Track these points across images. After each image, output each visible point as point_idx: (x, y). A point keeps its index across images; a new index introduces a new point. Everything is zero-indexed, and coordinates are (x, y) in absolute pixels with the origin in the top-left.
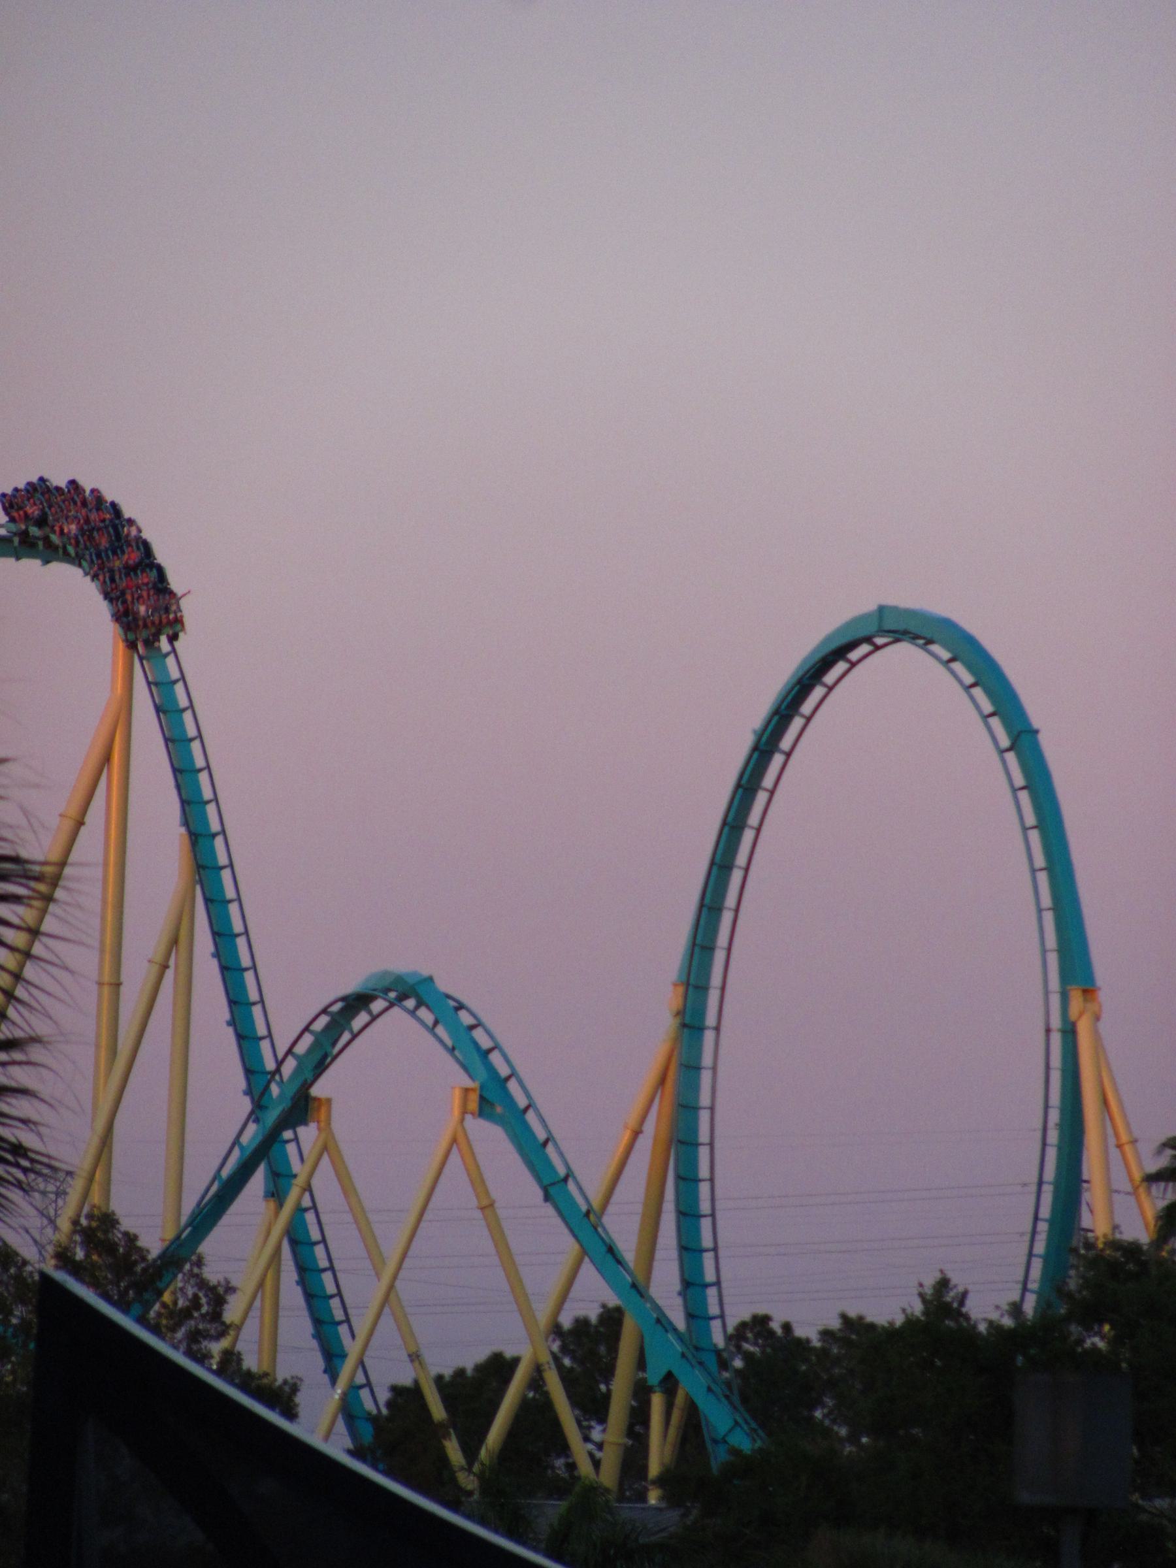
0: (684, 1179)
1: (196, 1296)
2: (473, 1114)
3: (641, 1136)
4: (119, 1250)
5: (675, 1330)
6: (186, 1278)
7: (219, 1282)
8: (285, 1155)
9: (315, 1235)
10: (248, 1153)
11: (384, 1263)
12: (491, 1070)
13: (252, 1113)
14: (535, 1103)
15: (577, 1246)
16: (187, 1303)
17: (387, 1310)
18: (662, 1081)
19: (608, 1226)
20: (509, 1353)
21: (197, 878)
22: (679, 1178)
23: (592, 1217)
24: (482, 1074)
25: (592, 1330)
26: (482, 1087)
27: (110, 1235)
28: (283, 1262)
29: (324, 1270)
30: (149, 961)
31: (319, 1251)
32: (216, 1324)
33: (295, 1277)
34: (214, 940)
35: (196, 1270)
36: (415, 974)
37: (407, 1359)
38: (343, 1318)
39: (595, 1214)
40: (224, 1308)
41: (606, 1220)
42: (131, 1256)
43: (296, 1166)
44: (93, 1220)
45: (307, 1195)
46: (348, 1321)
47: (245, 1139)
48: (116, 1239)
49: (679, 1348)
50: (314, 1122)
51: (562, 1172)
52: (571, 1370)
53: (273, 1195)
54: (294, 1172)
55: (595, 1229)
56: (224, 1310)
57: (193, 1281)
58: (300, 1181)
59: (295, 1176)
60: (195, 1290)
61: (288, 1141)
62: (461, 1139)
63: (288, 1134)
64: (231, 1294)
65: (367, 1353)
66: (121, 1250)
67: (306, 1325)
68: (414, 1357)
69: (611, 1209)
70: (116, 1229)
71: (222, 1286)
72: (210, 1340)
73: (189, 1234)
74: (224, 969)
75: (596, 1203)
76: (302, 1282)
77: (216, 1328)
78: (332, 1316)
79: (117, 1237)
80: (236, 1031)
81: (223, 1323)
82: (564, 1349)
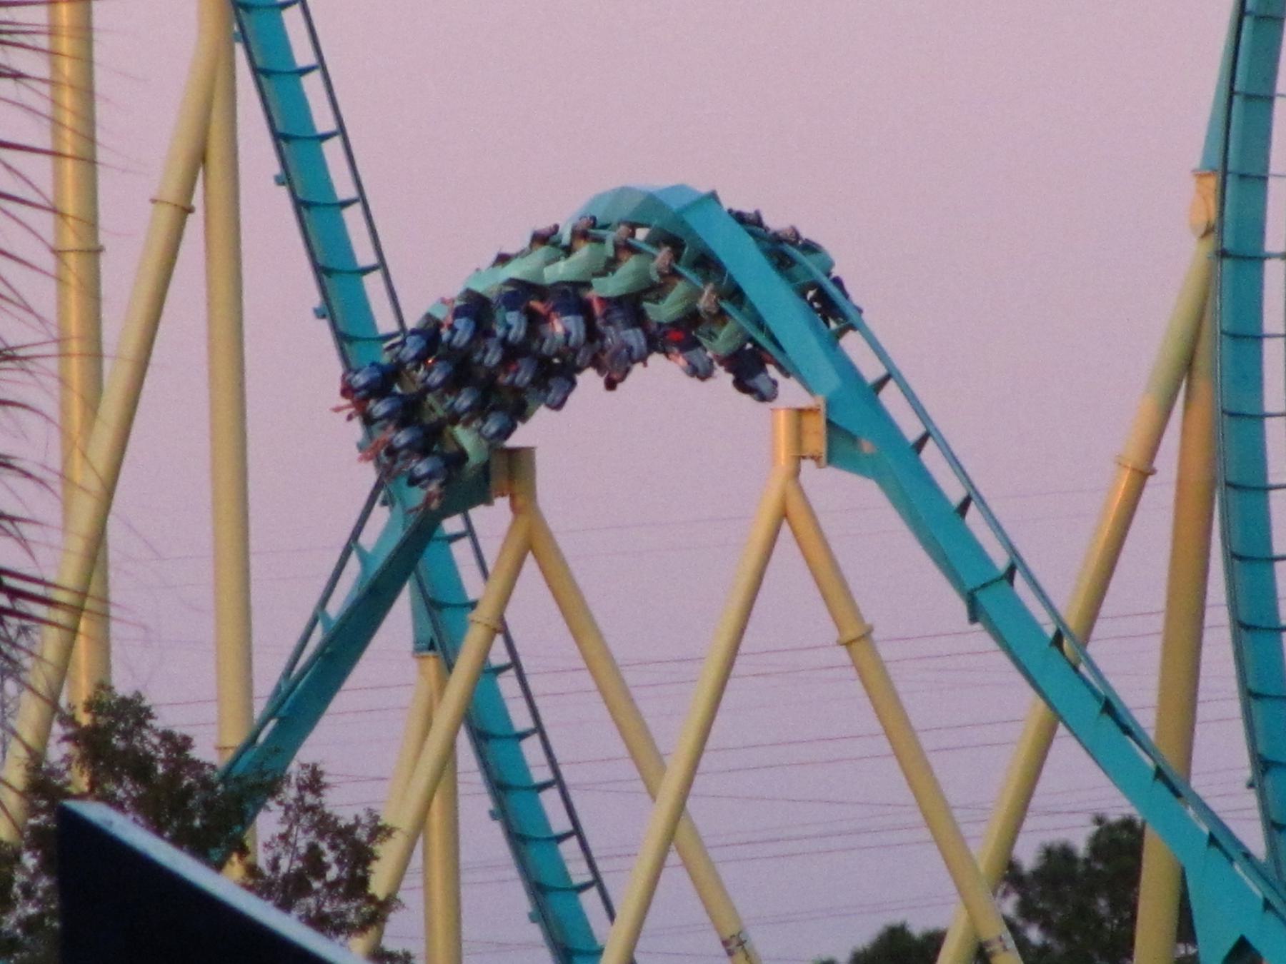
0: (1248, 627)
1: (313, 849)
2: (816, 458)
3: (1151, 480)
4: (155, 769)
5: (1247, 856)
6: (291, 814)
7: (356, 818)
8: (450, 562)
9: (521, 719)
10: (377, 564)
11: (662, 768)
12: (848, 370)
13: (378, 486)
14: (936, 430)
15: (1041, 704)
16: (298, 864)
17: (673, 858)
18: (1188, 365)
19: (1102, 665)
20: (918, 928)
21: (236, 28)
22: (1234, 557)
23: (1066, 644)
24: (830, 381)
25: (1081, 868)
26: (829, 405)
27: (136, 742)
28: (460, 777)
29: (544, 786)
30: (154, 201)
31: (531, 749)
32: (359, 901)
33: (487, 803)
34: (279, 149)
35: (310, 799)
36: (680, 189)
37: (722, 951)
38: (588, 878)
39: (1072, 637)
40: (369, 868)
41: (1092, 649)
42: (182, 778)
43: (473, 585)
44: (100, 713)
45: (499, 641)
46: (597, 881)
47: (368, 539)
48: (148, 748)
49: (1257, 891)
50: (503, 495)
51: (1001, 561)
52: (1044, 950)
53: (431, 647)
54: (471, 596)
55: (1076, 669)
56: (371, 872)
57: (305, 820)
58: (484, 614)
59: (473, 605)
60: (312, 836)
61: (456, 537)
62: (795, 507)
63: (452, 524)
64: (381, 841)
65: (641, 945)
66: (160, 769)
67: (519, 899)
68: (732, 947)
69: (1100, 628)
70: (147, 727)
71: (364, 826)
72: (349, 934)
73: (275, 731)
74: (301, 206)
75: (1072, 620)
76: (502, 813)
77: (358, 909)
78: (566, 875)
79: (150, 743)
80: (334, 326)
81: (372, 899)
82: (1027, 910)
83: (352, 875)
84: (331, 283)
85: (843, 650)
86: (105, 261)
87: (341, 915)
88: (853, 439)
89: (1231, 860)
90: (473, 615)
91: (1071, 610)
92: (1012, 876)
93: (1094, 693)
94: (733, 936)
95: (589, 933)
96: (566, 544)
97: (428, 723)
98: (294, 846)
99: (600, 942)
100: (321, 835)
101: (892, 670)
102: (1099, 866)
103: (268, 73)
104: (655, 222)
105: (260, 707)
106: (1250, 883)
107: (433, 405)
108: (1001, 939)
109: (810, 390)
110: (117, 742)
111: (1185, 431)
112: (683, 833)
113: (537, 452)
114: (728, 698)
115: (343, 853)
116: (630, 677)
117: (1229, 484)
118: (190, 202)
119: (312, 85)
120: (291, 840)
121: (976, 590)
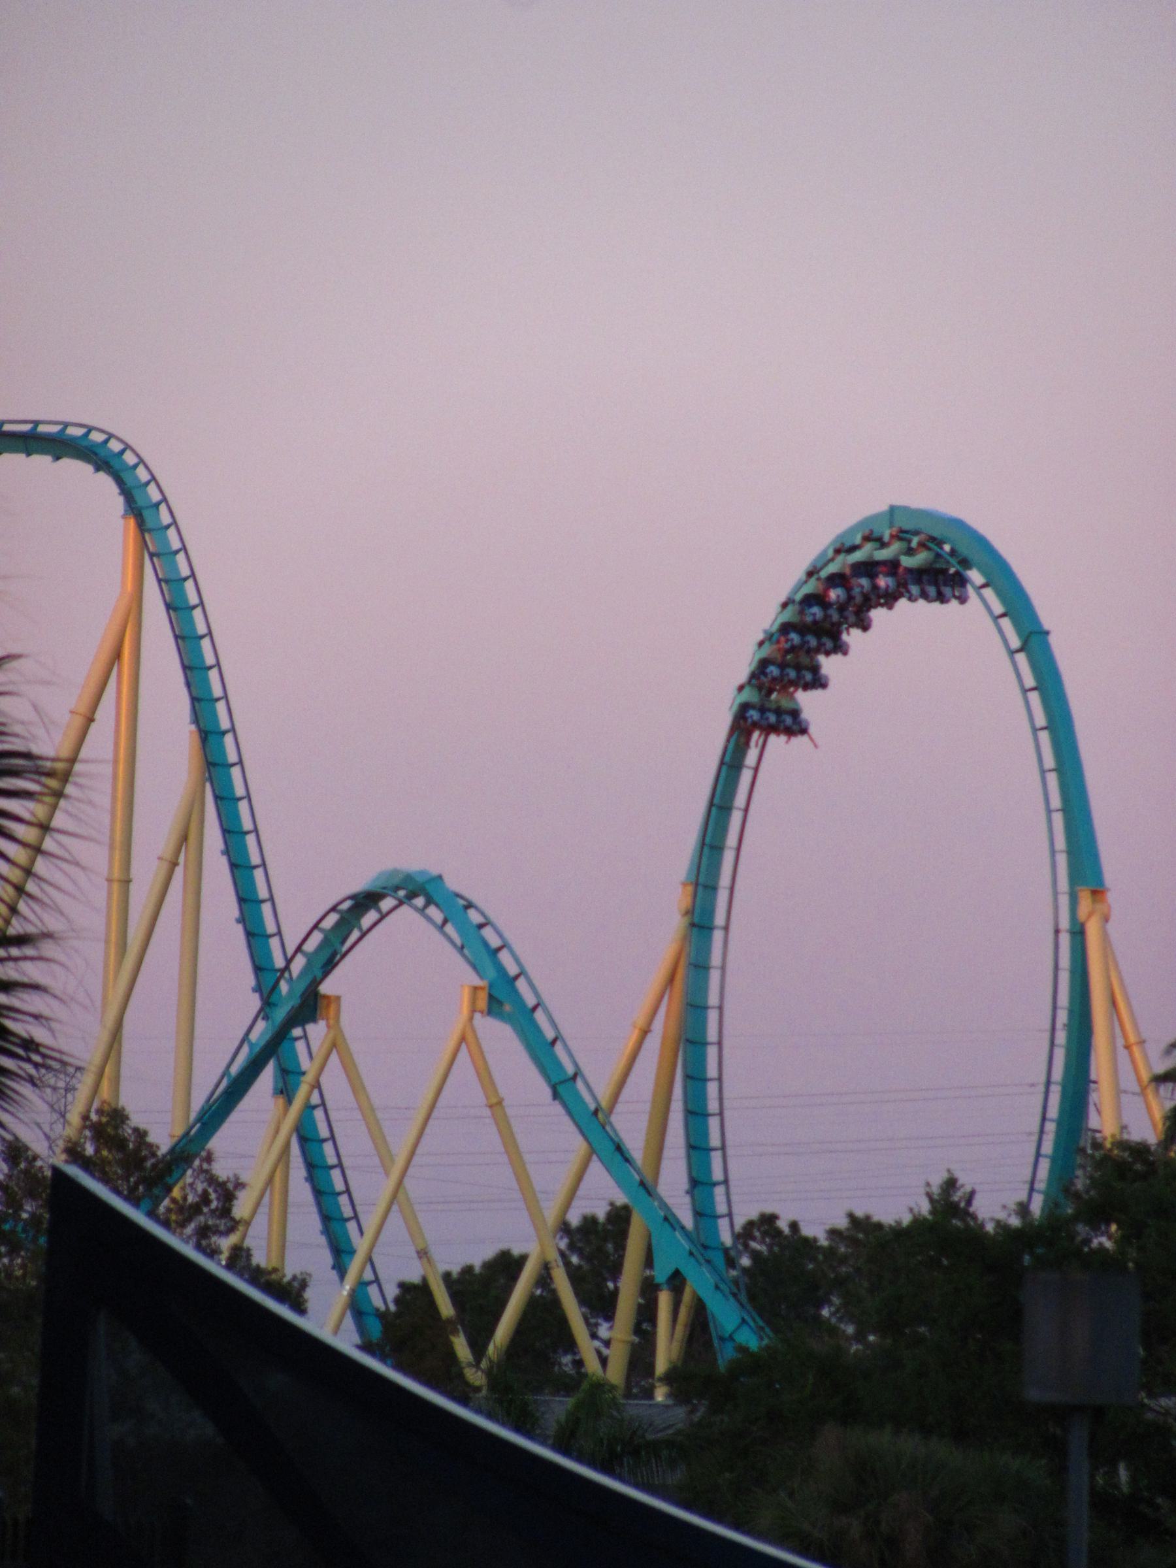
2: (482, 1012)
3: (649, 1035)
5: (683, 1228)
6: (195, 1173)
8: (294, 1050)
9: (324, 1133)
10: (257, 1049)
11: (393, 1161)
12: (501, 969)
18: (671, 980)
20: (516, 1251)
21: (207, 775)
22: (688, 1077)
24: (492, 973)
25: (600, 1228)
26: (491, 986)
27: (120, 1131)
30: (159, 858)
31: (328, 1148)
35: (205, 1166)
36: (422, 873)
40: (232, 1203)
43: (305, 1063)
47: (254, 1036)
48: (126, 1135)
49: (687, 1246)
52: (579, 1267)
53: (282, 1092)
55: (604, 1128)
57: (202, 1177)
58: (309, 1078)
59: (304, 1073)
60: (205, 1184)
62: (469, 1037)
63: (297, 1032)
65: (375, 1250)
66: (131, 1146)
69: (619, 1108)
73: (199, 1131)
74: (233, 866)
75: (604, 1104)
76: (311, 1179)
77: (225, 1224)
81: (233, 1219)
82: (572, 1246)
83: (223, 1206)
84: (245, 906)
85: (488, 1109)
86: (132, 886)
87: (217, 1226)
88: (500, 1003)
89: (674, 1229)
90: (304, 1078)
91: (604, 1098)
92: (565, 1228)
93: (612, 1139)
94: (422, 1250)
95: (349, 1240)
96: (354, 1047)
97: (277, 1131)
98: (196, 1190)
99: (355, 1247)
100: (210, 1185)
101: (513, 1122)
102: (610, 1227)
103: (222, 799)
104: (411, 887)
105: (193, 1116)
106: (683, 1242)
107: (320, 966)
108: (556, 1261)
109: (481, 978)
110: (110, 1130)
111: (668, 1011)
112: (401, 1196)
113: (342, 998)
114: (428, 1130)
115: (220, 1195)
116: (380, 1115)
117: (687, 1040)
118: (129, 876)
119: (243, 806)
120: (194, 1186)
121: (556, 1084)
